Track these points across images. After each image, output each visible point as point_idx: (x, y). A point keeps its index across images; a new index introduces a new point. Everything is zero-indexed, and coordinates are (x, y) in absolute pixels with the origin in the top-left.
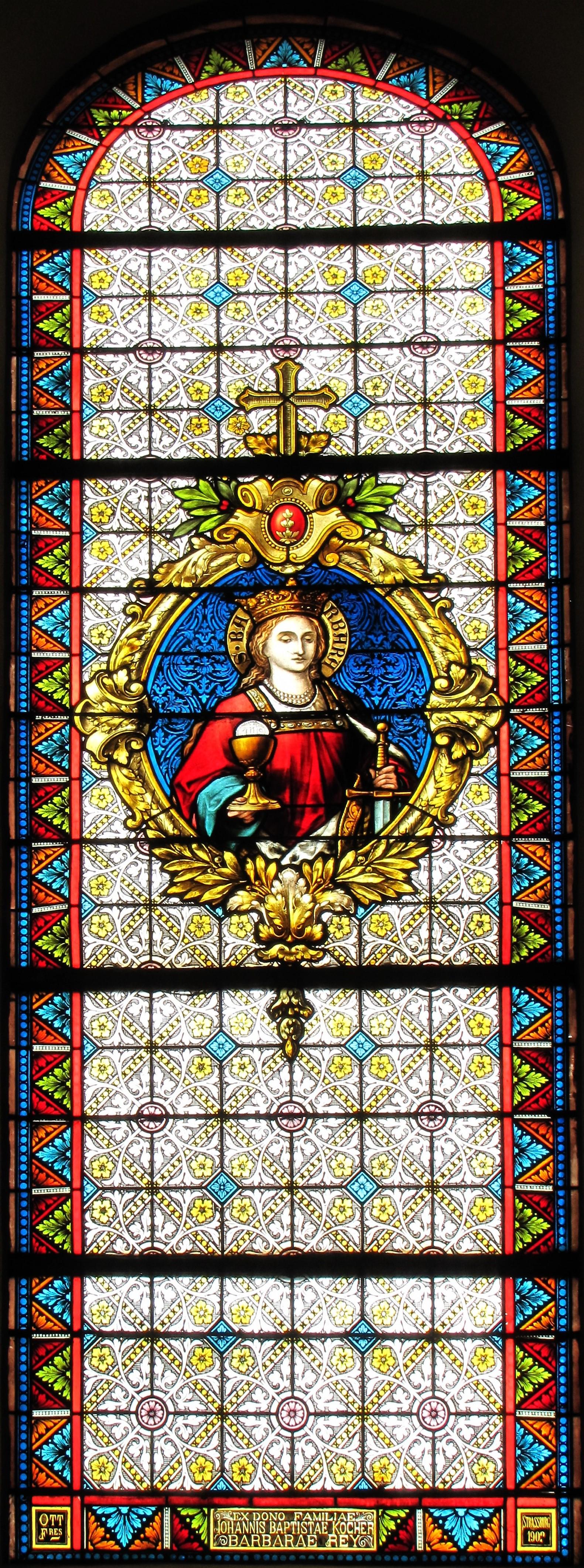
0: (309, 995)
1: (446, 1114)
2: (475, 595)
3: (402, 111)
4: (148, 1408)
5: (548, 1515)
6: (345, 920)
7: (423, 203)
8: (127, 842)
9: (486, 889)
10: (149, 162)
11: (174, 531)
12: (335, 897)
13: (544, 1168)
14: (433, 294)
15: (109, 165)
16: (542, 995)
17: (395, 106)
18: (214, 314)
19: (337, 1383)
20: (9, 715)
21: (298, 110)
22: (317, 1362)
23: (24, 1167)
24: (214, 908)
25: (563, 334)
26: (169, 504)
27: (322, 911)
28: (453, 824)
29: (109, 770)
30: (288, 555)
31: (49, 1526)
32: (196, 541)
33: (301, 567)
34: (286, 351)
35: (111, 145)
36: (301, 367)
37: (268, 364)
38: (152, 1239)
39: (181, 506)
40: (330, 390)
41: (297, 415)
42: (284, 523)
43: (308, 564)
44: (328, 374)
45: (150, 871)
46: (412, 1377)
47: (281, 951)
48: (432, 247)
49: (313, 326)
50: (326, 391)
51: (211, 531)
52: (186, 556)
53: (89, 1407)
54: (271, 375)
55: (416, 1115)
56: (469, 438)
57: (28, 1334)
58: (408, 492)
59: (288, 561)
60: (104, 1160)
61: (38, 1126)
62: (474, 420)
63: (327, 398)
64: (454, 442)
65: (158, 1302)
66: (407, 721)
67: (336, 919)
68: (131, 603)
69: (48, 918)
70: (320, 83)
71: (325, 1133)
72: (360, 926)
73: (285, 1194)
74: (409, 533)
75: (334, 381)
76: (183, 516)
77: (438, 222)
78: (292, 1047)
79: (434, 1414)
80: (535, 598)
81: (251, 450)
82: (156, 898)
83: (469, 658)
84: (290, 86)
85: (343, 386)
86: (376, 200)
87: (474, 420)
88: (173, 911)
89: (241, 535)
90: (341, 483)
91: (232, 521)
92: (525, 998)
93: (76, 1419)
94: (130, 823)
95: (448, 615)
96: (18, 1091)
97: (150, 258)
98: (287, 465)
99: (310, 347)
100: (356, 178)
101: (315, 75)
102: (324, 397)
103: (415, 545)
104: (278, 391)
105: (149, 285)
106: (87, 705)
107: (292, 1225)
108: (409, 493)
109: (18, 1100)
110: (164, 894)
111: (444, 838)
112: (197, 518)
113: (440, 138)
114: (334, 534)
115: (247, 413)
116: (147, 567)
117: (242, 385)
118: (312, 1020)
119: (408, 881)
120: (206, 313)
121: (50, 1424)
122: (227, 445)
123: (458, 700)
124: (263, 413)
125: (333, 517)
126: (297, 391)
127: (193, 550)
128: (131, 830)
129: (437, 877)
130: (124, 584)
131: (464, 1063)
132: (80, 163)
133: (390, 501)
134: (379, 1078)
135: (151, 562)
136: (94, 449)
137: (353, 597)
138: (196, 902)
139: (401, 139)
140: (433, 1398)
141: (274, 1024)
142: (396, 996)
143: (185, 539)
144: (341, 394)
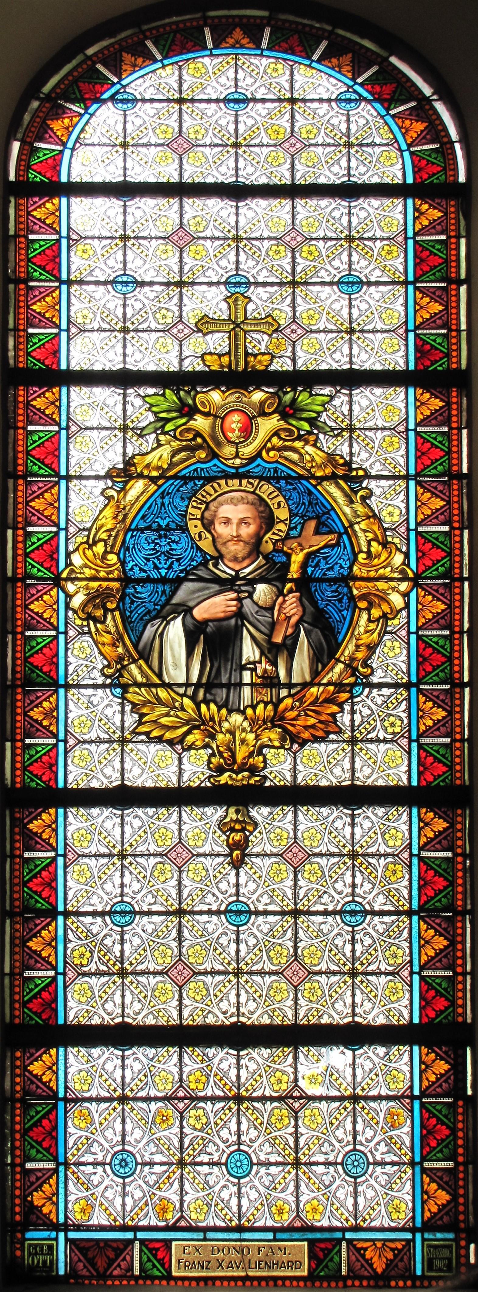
0: (254, 813)
1: (361, 283)
3: (332, 89)
4: (120, 1156)
7: (350, 308)
8: (103, 686)
11: (143, 429)
12: (273, 735)
14: (356, 148)
17: (325, 83)
20: (6, 579)
21: (248, 86)
25: (469, 907)
26: (140, 407)
27: (263, 746)
32: (162, 438)
36: (250, 300)
37: (222, 297)
38: (123, 1058)
39: (149, 409)
41: (245, 338)
45: (122, 712)
47: (230, 776)
50: (270, 319)
51: (175, 430)
52: (153, 450)
53: (72, 1160)
54: (224, 306)
55: (338, 283)
58: (336, 402)
59: (237, 456)
66: (334, 588)
68: (108, 488)
70: (264, 61)
73: (232, 978)
75: (277, 312)
78: (238, 854)
80: (441, 697)
81: (209, 366)
82: (127, 735)
84: (239, 63)
85: (283, 314)
90: (281, 394)
91: (192, 422)
97: (125, 175)
98: (237, 378)
100: (294, 241)
101: (261, 55)
104: (230, 319)
106: (72, 571)
108: (338, 404)
110: (133, 732)
112: (162, 419)
113: (364, 114)
116: (121, 459)
124: (217, 335)
126: (246, 319)
127: (159, 445)
128: (107, 677)
129: (358, 719)
130: (102, 473)
132: (67, 128)
138: (159, 740)
139: (331, 113)
140: (352, 1156)
141: (224, 837)
143: (154, 436)
144: (282, 322)
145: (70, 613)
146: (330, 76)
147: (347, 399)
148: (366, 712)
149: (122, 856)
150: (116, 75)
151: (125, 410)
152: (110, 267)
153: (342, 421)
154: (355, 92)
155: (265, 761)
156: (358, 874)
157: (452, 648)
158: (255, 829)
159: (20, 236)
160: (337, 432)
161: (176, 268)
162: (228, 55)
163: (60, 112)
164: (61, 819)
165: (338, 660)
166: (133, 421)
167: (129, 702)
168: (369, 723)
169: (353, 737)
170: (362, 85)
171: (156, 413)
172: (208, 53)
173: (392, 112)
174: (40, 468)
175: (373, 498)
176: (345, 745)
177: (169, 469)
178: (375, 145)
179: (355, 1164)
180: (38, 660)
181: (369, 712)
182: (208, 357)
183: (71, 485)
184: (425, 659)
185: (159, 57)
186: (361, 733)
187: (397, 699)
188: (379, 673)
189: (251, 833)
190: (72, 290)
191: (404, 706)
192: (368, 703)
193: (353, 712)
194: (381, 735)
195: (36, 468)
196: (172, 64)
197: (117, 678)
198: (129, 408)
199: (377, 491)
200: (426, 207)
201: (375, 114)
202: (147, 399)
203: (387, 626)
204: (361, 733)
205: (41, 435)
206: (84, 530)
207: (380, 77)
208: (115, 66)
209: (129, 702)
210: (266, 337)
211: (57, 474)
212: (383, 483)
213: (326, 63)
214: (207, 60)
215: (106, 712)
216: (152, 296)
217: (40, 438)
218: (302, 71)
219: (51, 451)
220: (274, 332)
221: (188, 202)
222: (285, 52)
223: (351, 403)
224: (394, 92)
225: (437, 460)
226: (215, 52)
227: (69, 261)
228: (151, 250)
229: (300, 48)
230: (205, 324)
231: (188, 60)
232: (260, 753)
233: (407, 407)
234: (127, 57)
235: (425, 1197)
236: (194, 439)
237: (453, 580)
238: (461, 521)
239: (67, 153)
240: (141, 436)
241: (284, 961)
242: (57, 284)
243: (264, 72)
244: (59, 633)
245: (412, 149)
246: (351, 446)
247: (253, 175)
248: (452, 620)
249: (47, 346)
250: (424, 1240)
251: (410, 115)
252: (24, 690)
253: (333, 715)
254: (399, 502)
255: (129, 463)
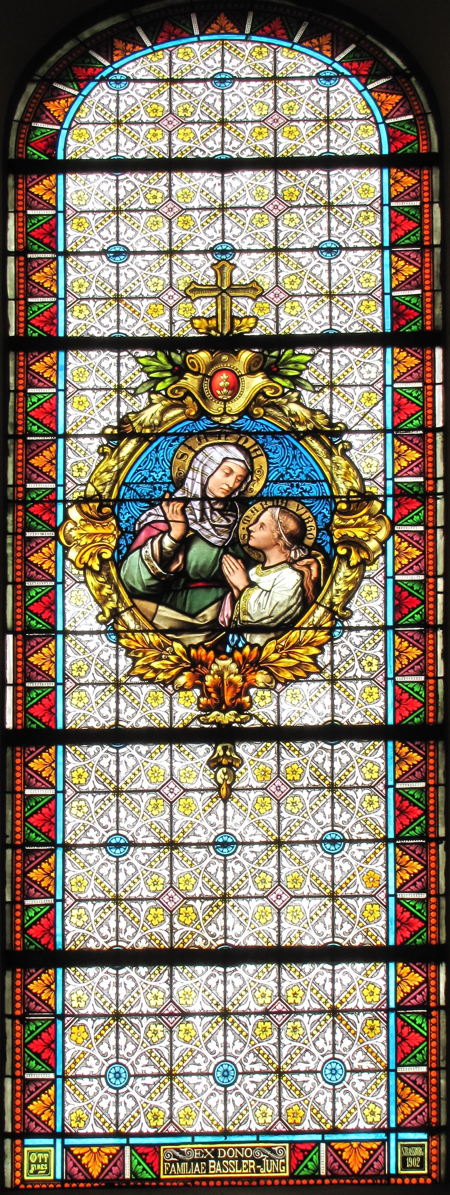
2: (368, 439)
3: (313, 68)
5: (422, 1146)
6: (267, 693)
9: (375, 775)
10: (118, 108)
11: (136, 389)
13: (420, 993)
15: (86, 110)
16: (418, 746)
18: (167, 226)
19: (260, 933)
21: (233, 66)
22: (244, 917)
23: (18, 998)
24: (166, 685)
28: (350, 617)
29: (85, 575)
30: (225, 408)
31: (37, 1162)
32: (153, 396)
33: (236, 418)
34: (223, 254)
35: (89, 94)
36: (235, 266)
37: (208, 265)
40: (258, 284)
41: (232, 303)
42: (222, 384)
43: (240, 415)
44: (255, 271)
45: (117, 656)
46: (317, 1043)
48: (335, 172)
49: (243, 65)
51: (166, 390)
54: (211, 273)
56: (364, 321)
57: (24, 437)
58: (318, 360)
60: (80, 770)
61: (30, 638)
62: (368, 307)
63: (255, 289)
64: (353, 324)
65: (122, 767)
67: (260, 693)
69: (40, 262)
71: (251, 857)
72: (278, 697)
74: (318, 392)
76: (144, 377)
77: (340, 153)
79: (334, 1072)
83: (363, 486)
85: (267, 280)
86: (294, 313)
87: (368, 307)
88: (135, 689)
89: (188, 393)
92: (406, 749)
93: (59, 1081)
94: (101, 618)
95: (348, 453)
96: (14, 771)
99: (241, 251)
100: (279, 896)
101: (246, 40)
102: (254, 290)
103: (322, 401)
104: (216, 284)
105: (118, 290)
107: (225, 1043)
108: (319, 364)
109: (14, 832)
110: (128, 675)
111: (343, 628)
112: (152, 379)
113: (343, 90)
114: (261, 392)
115: (193, 301)
116: (115, 417)
117: (188, 280)
118: (242, 769)
119: (315, 663)
120: (161, 224)
121: (39, 692)
122: (177, 325)
123: (355, 519)
124: (205, 301)
125: (258, 381)
129: (337, 659)
130: (97, 431)
131: (357, 692)
133: (303, 367)
134: (293, 1040)
135: (119, 413)
136: (75, 328)
137: (275, 441)
138: (151, 681)
142: (307, 971)
145: (68, 563)
146: (312, 57)
147: (328, 357)
148: (345, 652)
149: (117, 900)
150: (107, 59)
151: (119, 372)
152: (104, 238)
153: (324, 378)
154: (334, 70)
155: (251, 701)
156: (337, 805)
157: (426, 801)
158: (241, 766)
159: (18, 486)
160: (316, 389)
161: (166, 238)
162: (216, 40)
163: (55, 93)
164: (61, 362)
165: (319, 604)
166: (126, 382)
167: (123, 647)
168: (348, 663)
169: (333, 675)
170: (340, 63)
171: (148, 373)
172: (195, 39)
173: (370, 87)
174: (39, 428)
175: (352, 451)
176: (325, 684)
177: (161, 424)
178: (353, 119)
179: (335, 1073)
180: (37, 711)
181: (348, 652)
182: (197, 322)
183: (68, 443)
184: (404, 1039)
185: (149, 44)
186: (340, 672)
187: (374, 639)
188: (357, 616)
189: (238, 768)
190: (67, 640)
191: (381, 646)
192: (347, 643)
193: (333, 652)
194: (360, 673)
195: (35, 428)
196: (162, 50)
197: (112, 624)
198: (123, 370)
199: (356, 444)
200: (401, 174)
201: (353, 90)
202: (141, 360)
203: (365, 571)
204: (340, 672)
205: (40, 396)
206: (82, 485)
207: (358, 55)
208: (107, 52)
209: (123, 647)
210: (251, 302)
211: (55, 433)
212: (362, 436)
213: (307, 44)
214: (195, 46)
215: (101, 871)
216: (143, 265)
217: (39, 400)
218: (285, 54)
219: (47, 815)
220: (258, 296)
221: (176, 177)
222: (268, 36)
223: (331, 361)
224: (371, 68)
225: (413, 415)
226: (202, 38)
227: (65, 234)
228: (142, 222)
229: (282, 31)
230: (193, 291)
231: (177, 46)
232: (247, 694)
233: (387, 872)
234: (119, 44)
235: (399, 979)
236: (184, 397)
237: (423, 247)
238: (431, 197)
239: (64, 133)
240: (135, 395)
241: (265, 216)
242: (54, 256)
243: (247, 54)
244: (57, 583)
245: (388, 122)
246: (331, 402)
247: (237, 149)
248: (426, 565)
249: (46, 314)
250: (397, 1140)
251: (387, 88)
252: (24, 850)
253: (314, 657)
254: (378, 651)
255: (123, 421)
